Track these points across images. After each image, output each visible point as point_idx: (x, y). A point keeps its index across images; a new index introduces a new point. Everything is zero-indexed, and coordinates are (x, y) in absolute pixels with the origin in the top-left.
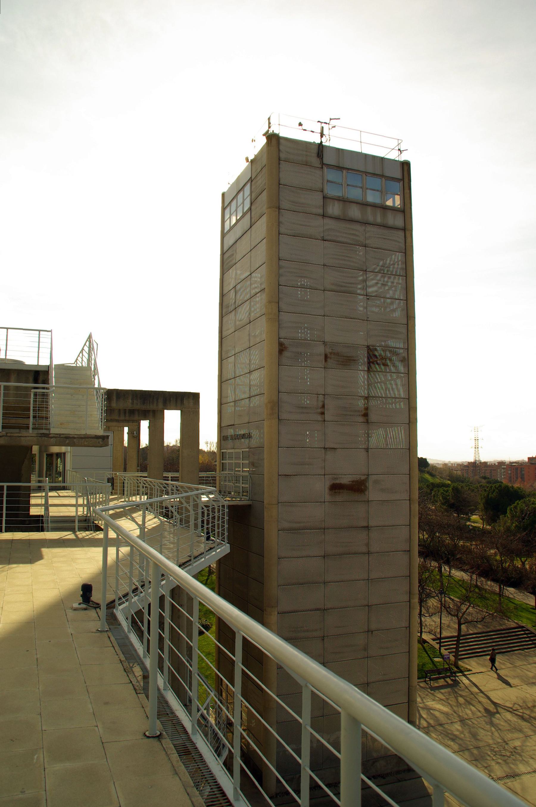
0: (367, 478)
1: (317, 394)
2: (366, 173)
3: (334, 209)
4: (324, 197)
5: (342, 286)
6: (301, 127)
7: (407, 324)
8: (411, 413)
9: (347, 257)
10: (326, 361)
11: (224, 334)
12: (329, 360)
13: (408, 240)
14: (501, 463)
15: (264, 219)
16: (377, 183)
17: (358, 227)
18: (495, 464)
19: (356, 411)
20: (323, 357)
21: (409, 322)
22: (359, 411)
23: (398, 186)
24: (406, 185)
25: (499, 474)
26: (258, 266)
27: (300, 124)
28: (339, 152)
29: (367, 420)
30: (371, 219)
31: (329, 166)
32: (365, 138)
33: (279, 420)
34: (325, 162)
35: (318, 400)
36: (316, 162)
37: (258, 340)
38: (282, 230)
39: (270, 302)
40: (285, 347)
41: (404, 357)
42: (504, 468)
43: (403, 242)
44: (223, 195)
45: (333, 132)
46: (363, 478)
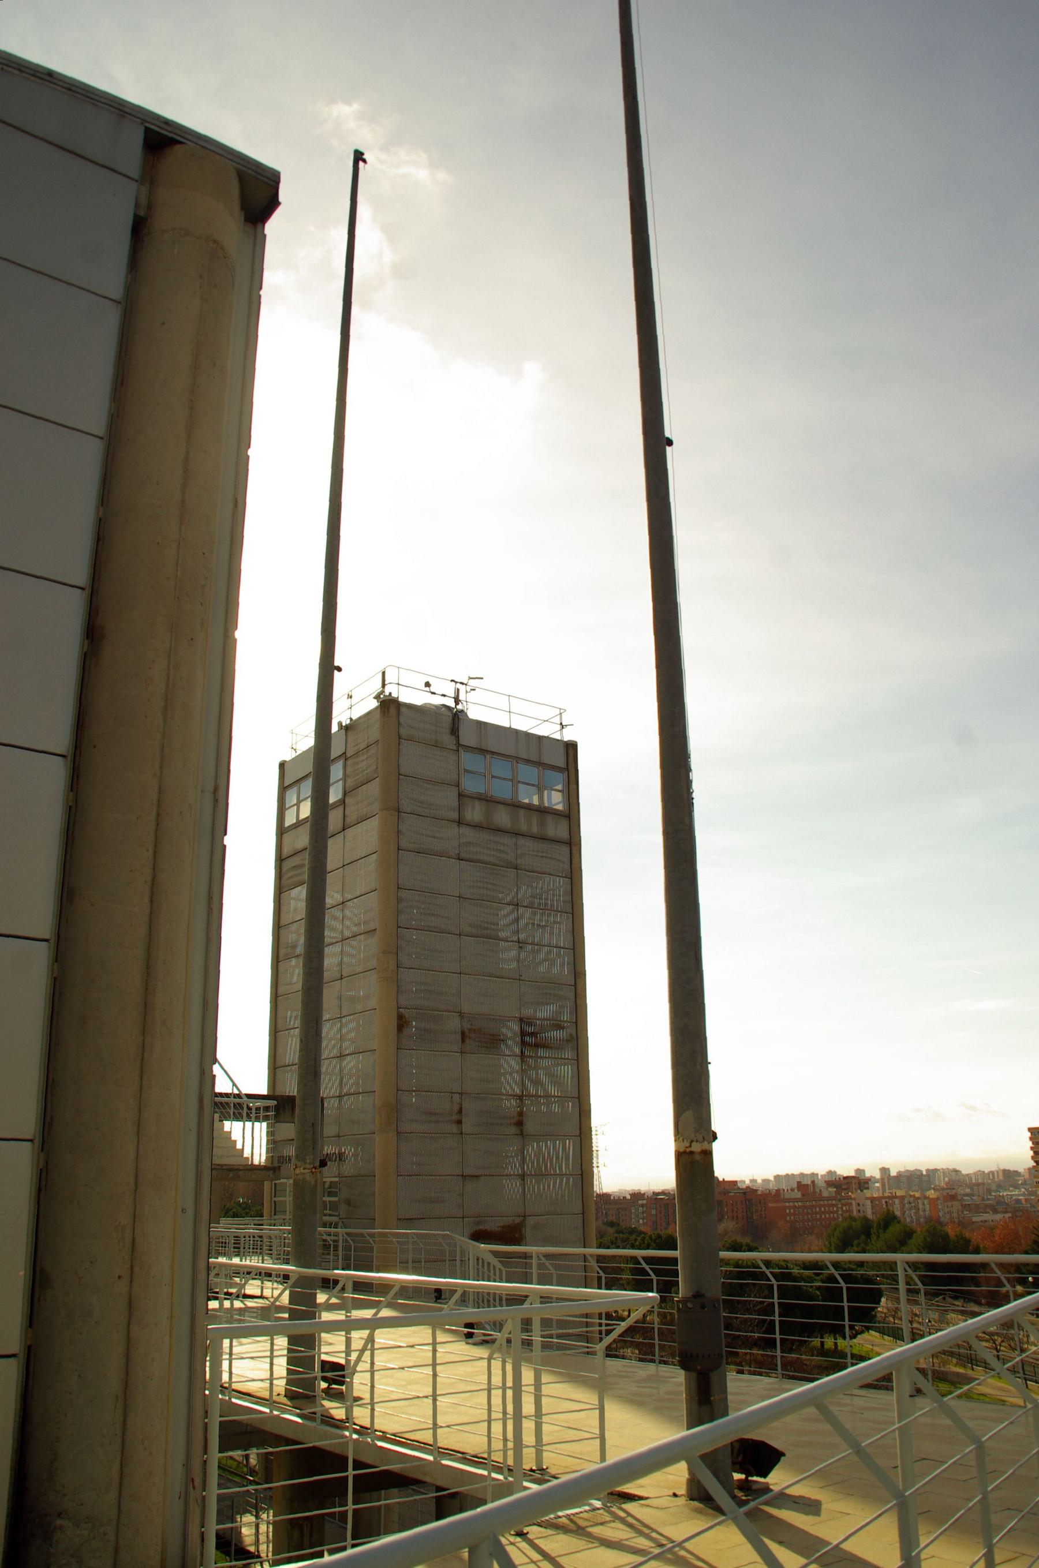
0: (523, 1222)
2: (518, 759)
3: (475, 813)
4: (460, 795)
5: (484, 928)
6: (427, 689)
7: (575, 985)
10: (463, 1041)
11: (282, 990)
12: (467, 1041)
13: (575, 860)
14: (637, 1196)
15: (374, 823)
16: (529, 773)
18: (624, 1198)
20: (459, 1037)
23: (560, 777)
24: (572, 777)
26: (358, 894)
27: (428, 684)
28: (481, 725)
29: (522, 1131)
30: (524, 827)
31: (468, 748)
32: (517, 706)
34: (461, 742)
35: (452, 1101)
36: (448, 740)
37: (360, 1007)
38: (404, 844)
41: (571, 1035)
42: (642, 1206)
43: (567, 860)
44: (282, 765)
45: (471, 697)
46: (518, 1220)
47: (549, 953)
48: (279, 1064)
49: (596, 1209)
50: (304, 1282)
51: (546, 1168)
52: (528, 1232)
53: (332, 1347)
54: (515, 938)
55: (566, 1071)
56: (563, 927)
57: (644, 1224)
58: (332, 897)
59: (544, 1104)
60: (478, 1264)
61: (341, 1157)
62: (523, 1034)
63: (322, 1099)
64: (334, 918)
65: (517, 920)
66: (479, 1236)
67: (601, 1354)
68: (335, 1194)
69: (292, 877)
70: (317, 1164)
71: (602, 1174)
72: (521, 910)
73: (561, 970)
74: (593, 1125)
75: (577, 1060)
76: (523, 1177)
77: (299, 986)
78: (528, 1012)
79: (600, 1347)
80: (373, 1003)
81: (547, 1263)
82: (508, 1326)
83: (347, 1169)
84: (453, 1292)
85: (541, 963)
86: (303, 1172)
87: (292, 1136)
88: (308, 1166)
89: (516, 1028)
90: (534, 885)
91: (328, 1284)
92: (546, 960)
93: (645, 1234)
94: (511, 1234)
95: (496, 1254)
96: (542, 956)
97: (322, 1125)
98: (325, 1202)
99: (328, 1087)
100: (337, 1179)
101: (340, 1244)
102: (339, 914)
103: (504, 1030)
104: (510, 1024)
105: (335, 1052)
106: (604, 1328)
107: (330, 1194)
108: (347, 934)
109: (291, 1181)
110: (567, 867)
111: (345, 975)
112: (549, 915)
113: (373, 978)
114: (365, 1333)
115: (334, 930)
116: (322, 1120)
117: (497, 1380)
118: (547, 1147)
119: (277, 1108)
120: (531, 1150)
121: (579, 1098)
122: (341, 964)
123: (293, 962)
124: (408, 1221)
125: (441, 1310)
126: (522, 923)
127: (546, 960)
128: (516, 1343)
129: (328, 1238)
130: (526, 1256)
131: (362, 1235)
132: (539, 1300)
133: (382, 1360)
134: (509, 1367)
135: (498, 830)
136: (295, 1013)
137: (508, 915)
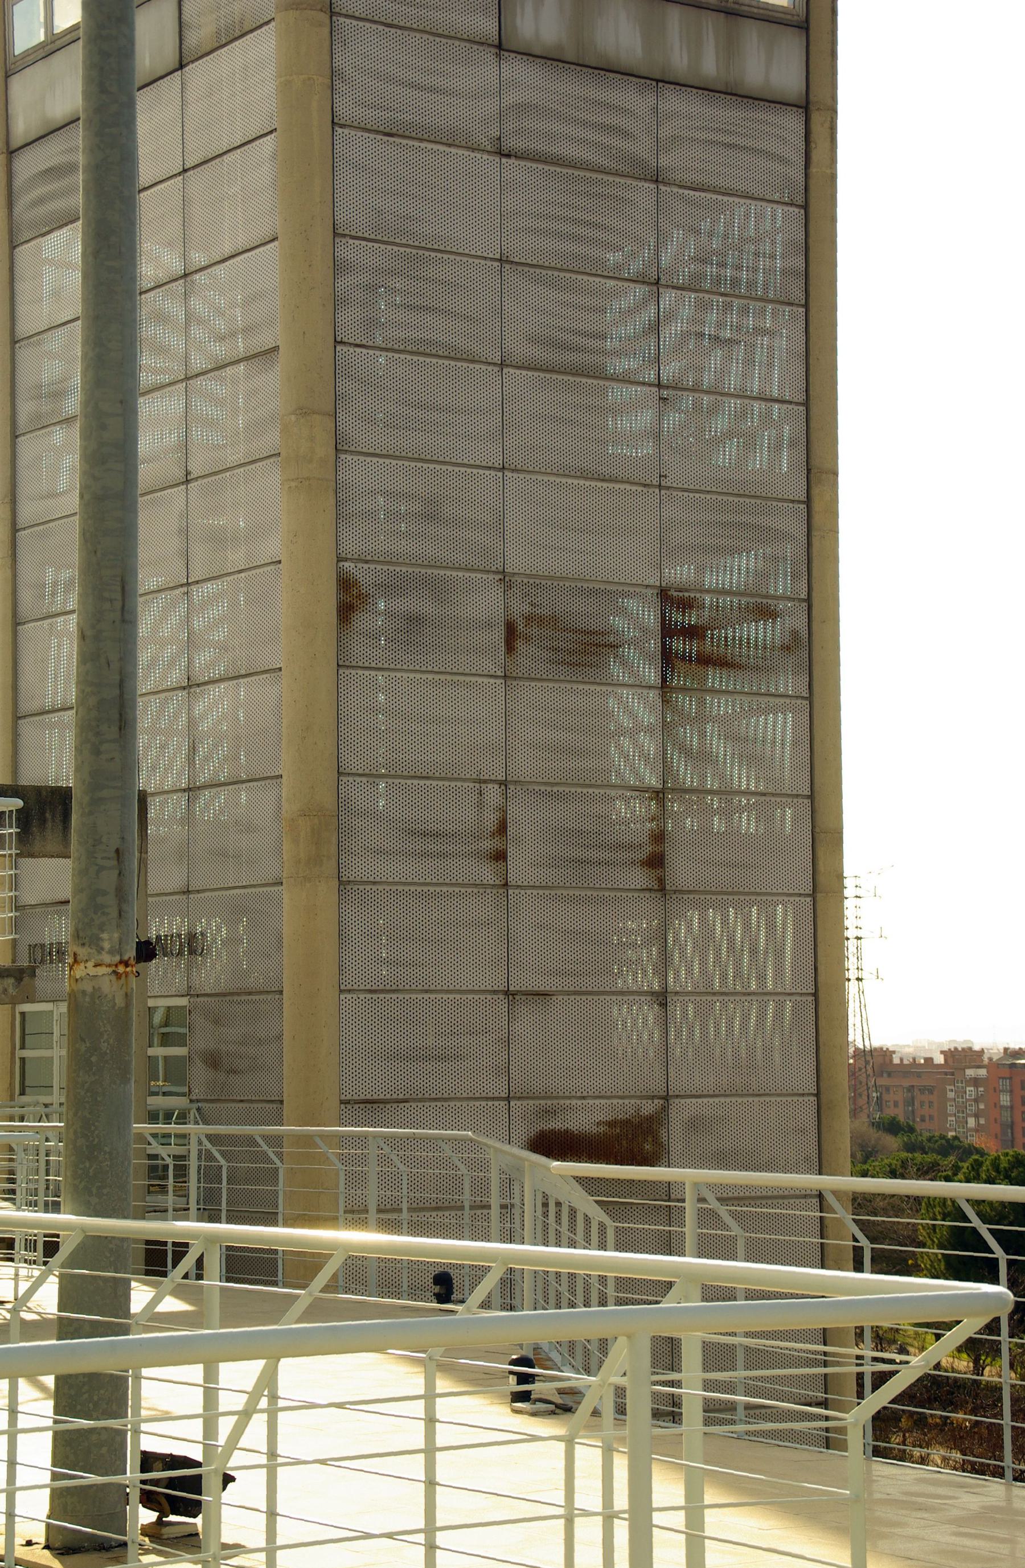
0: (665, 1109)
1: (480, 781)
7: (808, 502)
8: (820, 853)
9: (588, 224)
10: (510, 647)
14: (961, 1058)
15: (263, 48)
17: (636, 100)
18: (929, 1060)
19: (619, 846)
20: (498, 635)
21: (815, 491)
22: (631, 847)
25: (951, 1109)
26: (228, 249)
29: (661, 881)
30: (679, 61)
33: (342, 883)
35: (480, 805)
37: (237, 558)
38: (345, 109)
39: (303, 412)
40: (359, 596)
42: (976, 1082)
46: (648, 1108)
47: (742, 415)
48: (25, 707)
49: (854, 1088)
50: (97, 1250)
51: (724, 977)
52: (675, 1134)
53: (167, 1411)
54: (651, 376)
55: (780, 728)
56: (782, 343)
57: (978, 1129)
58: (156, 258)
59: (719, 811)
60: (546, 1214)
61: (192, 945)
62: (667, 631)
63: (143, 798)
64: (162, 318)
65: (655, 328)
66: (553, 1144)
67: (857, 1439)
68: (179, 1040)
69: (41, 201)
70: (131, 953)
71: (869, 998)
72: (668, 298)
73: (774, 463)
74: (848, 870)
75: (810, 699)
76: (662, 998)
77: (72, 502)
78: (680, 573)
79: (857, 1418)
80: (273, 546)
81: (723, 1210)
82: (620, 1354)
83: (212, 973)
84: (479, 1273)
85: (718, 441)
86: (93, 971)
87: (65, 890)
88: (107, 958)
89: (651, 618)
90: (705, 226)
91: (157, 1259)
92: (730, 434)
93: (982, 1153)
94: (633, 1139)
95: (587, 1183)
96: (720, 424)
97: (143, 863)
98: (152, 1060)
99: (158, 763)
100: (183, 1002)
101: (193, 1164)
102: (176, 309)
103: (618, 622)
104: (632, 604)
105: (176, 676)
106: (868, 1369)
107: (166, 1040)
108: (198, 363)
109: (63, 1007)
110: (797, 174)
111: (196, 471)
112: (744, 311)
113: (271, 483)
114: (255, 1367)
115: (161, 350)
116: (143, 849)
117: (589, 1495)
118: (726, 923)
119: (24, 818)
120: (686, 928)
121: (811, 797)
122: (185, 446)
123: (58, 436)
124: (369, 1107)
125: (452, 1312)
126: (671, 332)
127: (730, 434)
128: (640, 1407)
129: (163, 1151)
130: (668, 1190)
131: (251, 1141)
132: (698, 1293)
133: (296, 1434)
134: (621, 1466)
135: (608, 69)
136: (66, 574)
137: (631, 312)
